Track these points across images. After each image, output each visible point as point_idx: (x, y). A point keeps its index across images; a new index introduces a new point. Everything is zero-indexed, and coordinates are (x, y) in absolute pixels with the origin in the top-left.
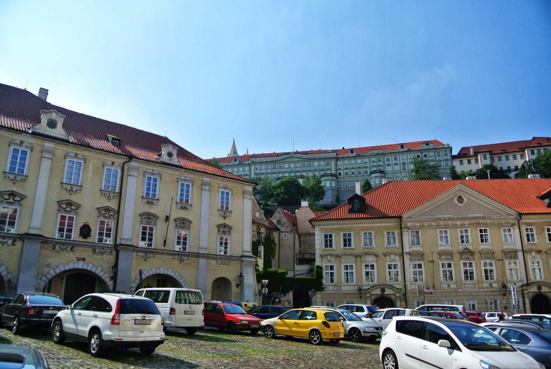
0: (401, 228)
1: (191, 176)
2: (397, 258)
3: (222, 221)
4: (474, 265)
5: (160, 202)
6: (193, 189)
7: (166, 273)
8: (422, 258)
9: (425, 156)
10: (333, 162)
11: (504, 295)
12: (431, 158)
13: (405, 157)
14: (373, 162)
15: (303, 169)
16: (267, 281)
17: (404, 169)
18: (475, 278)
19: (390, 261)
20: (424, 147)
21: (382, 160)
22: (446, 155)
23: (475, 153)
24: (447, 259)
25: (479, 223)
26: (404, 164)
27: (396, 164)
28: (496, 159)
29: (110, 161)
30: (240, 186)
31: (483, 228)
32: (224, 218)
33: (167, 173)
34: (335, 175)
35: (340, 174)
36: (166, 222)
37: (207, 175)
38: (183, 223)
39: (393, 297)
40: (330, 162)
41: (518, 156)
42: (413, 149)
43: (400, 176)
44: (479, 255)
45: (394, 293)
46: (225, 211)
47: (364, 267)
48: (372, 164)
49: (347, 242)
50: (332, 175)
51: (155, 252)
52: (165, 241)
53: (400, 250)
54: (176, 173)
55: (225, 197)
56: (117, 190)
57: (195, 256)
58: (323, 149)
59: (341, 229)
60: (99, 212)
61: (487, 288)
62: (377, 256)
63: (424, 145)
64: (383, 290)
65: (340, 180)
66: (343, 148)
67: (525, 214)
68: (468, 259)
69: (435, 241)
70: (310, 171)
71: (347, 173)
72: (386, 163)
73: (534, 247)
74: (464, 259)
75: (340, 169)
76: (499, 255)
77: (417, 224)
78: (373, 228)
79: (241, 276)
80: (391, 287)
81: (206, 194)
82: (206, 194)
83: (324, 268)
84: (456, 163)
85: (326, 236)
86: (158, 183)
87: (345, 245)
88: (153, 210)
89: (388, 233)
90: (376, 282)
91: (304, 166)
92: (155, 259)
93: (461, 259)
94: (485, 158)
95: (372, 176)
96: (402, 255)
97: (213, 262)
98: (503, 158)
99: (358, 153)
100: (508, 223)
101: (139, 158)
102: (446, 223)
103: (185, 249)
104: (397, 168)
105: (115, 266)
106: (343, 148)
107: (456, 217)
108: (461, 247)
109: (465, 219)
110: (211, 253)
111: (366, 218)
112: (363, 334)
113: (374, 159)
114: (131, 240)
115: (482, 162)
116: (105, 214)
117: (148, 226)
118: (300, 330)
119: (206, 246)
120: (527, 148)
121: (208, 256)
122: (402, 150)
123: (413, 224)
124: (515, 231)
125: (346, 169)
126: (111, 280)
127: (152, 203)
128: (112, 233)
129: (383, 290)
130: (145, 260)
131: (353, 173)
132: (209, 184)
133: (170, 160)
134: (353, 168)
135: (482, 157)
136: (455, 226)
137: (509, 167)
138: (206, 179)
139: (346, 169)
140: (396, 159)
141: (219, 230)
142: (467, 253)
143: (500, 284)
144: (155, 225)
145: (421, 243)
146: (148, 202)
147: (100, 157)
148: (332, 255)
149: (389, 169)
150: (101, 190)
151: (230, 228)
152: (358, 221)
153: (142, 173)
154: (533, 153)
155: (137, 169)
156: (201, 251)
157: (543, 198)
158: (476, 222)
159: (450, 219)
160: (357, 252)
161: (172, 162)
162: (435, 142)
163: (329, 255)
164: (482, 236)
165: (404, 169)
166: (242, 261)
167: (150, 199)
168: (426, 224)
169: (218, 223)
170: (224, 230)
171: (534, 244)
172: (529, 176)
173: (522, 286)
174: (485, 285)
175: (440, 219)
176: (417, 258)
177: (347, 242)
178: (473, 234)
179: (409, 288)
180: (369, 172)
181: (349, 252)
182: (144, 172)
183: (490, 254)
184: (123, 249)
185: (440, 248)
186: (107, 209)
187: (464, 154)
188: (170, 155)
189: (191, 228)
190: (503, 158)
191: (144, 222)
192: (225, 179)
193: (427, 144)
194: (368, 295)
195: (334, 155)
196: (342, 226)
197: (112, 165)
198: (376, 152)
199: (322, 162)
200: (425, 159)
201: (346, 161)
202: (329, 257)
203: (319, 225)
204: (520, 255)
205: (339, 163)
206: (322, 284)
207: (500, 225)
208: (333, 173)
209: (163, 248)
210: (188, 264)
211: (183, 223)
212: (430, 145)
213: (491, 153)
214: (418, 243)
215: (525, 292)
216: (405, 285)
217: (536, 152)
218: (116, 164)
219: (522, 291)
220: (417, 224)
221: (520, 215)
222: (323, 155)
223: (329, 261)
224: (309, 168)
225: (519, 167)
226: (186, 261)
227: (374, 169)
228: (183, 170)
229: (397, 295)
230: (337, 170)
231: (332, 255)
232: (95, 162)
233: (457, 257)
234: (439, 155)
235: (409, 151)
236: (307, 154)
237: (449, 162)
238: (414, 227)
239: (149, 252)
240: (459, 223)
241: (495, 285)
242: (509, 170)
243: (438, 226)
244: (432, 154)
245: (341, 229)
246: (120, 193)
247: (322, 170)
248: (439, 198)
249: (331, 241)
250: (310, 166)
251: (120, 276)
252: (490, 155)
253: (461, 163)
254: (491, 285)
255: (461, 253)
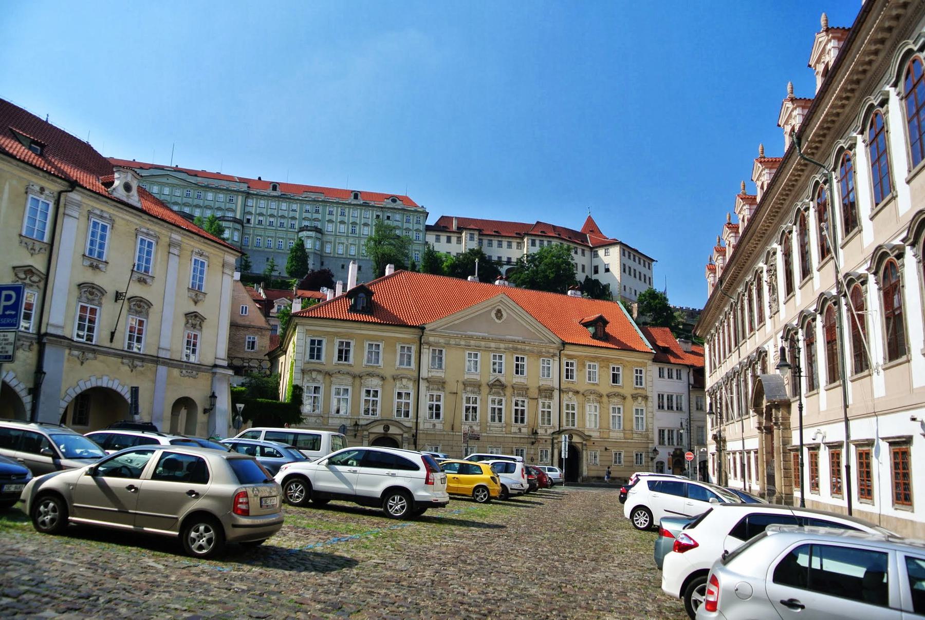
0: (421, 344)
1: (155, 228)
2: (411, 385)
3: (192, 308)
4: (503, 402)
5: (109, 267)
6: (156, 252)
7: (110, 386)
8: (443, 388)
9: (388, 218)
10: (240, 198)
11: (533, 443)
12: (396, 224)
13: (357, 213)
14: (307, 211)
15: (185, 200)
16: (242, 406)
17: (353, 232)
18: (526, 420)
19: (400, 388)
20: (388, 203)
21: (320, 211)
22: (418, 222)
23: (458, 228)
24: (474, 393)
25: (516, 349)
26: (354, 224)
27: (342, 222)
28: (485, 242)
29: (38, 185)
30: (220, 254)
31: (520, 356)
32: (196, 303)
33: (124, 219)
34: (239, 222)
35: (248, 221)
36: (116, 301)
37: (178, 230)
38: (140, 306)
39: (399, 438)
40: (234, 199)
41: (514, 245)
42: (372, 203)
43: (345, 241)
44: (511, 390)
45: (400, 432)
46: (197, 292)
47: (363, 393)
48: (305, 215)
49: (343, 354)
50: (235, 220)
51: (96, 351)
52: (113, 334)
53: (416, 374)
54: (136, 221)
55: (199, 269)
56: (46, 239)
57: (152, 361)
58: (225, 172)
59: (336, 334)
60: (16, 275)
61: (515, 433)
62: (383, 379)
63: (390, 201)
64: (387, 428)
65: (247, 231)
66: (260, 178)
67: (569, 344)
68: (498, 394)
69: (462, 366)
70: (197, 206)
71: (260, 222)
72: (328, 217)
73: (572, 386)
74: (494, 394)
75: (250, 213)
76: (534, 393)
77: (442, 341)
78: (382, 339)
79: (213, 396)
80: (398, 424)
81: (174, 261)
82: (174, 261)
83: (305, 390)
84: (431, 238)
85: (313, 342)
86: (108, 233)
87: (340, 358)
88: (99, 280)
89: (403, 348)
90: (378, 416)
91: (188, 196)
92: (95, 362)
93: (489, 393)
94: (472, 239)
95: (301, 234)
96: (417, 381)
97: (176, 372)
98: (495, 243)
99: (283, 192)
100: (548, 352)
101: (85, 188)
102: (478, 343)
103: (90, 338)
104: (343, 228)
105: (39, 372)
106: (260, 178)
107: (491, 337)
108: (492, 378)
109: (502, 341)
110: (174, 358)
111: (375, 323)
112: (510, 491)
113: (308, 207)
114: (62, 327)
115: (464, 245)
116: (25, 279)
117: (90, 306)
118: (460, 486)
119: (167, 346)
120: (528, 234)
121: (170, 363)
122: (355, 202)
123: (437, 339)
124: (554, 365)
125: (261, 214)
126: (29, 394)
127: (97, 267)
128: (33, 312)
129: (387, 428)
130: (82, 363)
131: (271, 224)
132: (180, 246)
133: (128, 197)
134: (272, 216)
135: (468, 236)
136: (488, 349)
137: (500, 258)
138: (176, 237)
139: (261, 214)
140: (343, 214)
141: (187, 322)
142: (498, 386)
143: (530, 429)
144: (100, 304)
145: (443, 367)
146: (91, 266)
147: (22, 175)
148: (319, 372)
149: (330, 227)
150: (20, 235)
151: (203, 319)
152: (363, 326)
153: (85, 213)
154: (533, 244)
155: (79, 205)
156: (162, 354)
157: (587, 325)
158: (515, 347)
159: (484, 339)
160: (356, 370)
161: (131, 202)
162: (405, 199)
163: (314, 370)
164: (517, 366)
165: (353, 232)
166: (214, 373)
167: (95, 261)
168: (452, 342)
169: (187, 312)
170: (194, 322)
171: (573, 383)
172: (569, 292)
173: (553, 433)
174: (514, 429)
175: (471, 337)
176: (436, 387)
177: (343, 354)
178: (508, 363)
179: (421, 426)
180: (297, 226)
181: (344, 369)
182: (89, 212)
183: (523, 390)
184: (51, 342)
185: (466, 377)
186: (30, 271)
187: (442, 226)
188: (127, 187)
189: (150, 314)
190: (495, 243)
191: (84, 299)
192: (202, 240)
193: (394, 201)
194: (366, 433)
195: (244, 187)
196: (339, 330)
197: (42, 193)
198: (313, 196)
199: (221, 196)
200: (386, 222)
201: (262, 202)
202: (314, 375)
203: (303, 325)
204: (556, 394)
205: (250, 202)
206: (299, 412)
207: (540, 355)
208: (238, 217)
209: (108, 344)
210: (142, 373)
211: (140, 306)
212: (398, 202)
213: (480, 232)
214: (440, 367)
215: (555, 441)
216: (417, 423)
217: (537, 242)
218: (47, 192)
219: (553, 440)
220: (442, 341)
221: (564, 344)
222: (225, 184)
223: (314, 380)
224: (196, 202)
225: (514, 260)
226: (139, 368)
227: (306, 223)
228: (146, 217)
229: (405, 435)
230: (245, 213)
231: (319, 372)
232: (14, 182)
233: (485, 390)
234: (408, 221)
235: (366, 205)
236: (196, 176)
237: (421, 235)
238: (437, 344)
239: (87, 349)
240: (493, 345)
241: (524, 430)
242: (499, 262)
243: (468, 346)
244: (398, 217)
245: (336, 334)
246: (51, 244)
247: (219, 209)
248: (475, 308)
249: (319, 350)
250: (199, 197)
251: (45, 388)
252: (480, 235)
253: (438, 239)
254: (520, 429)
255: (491, 386)
